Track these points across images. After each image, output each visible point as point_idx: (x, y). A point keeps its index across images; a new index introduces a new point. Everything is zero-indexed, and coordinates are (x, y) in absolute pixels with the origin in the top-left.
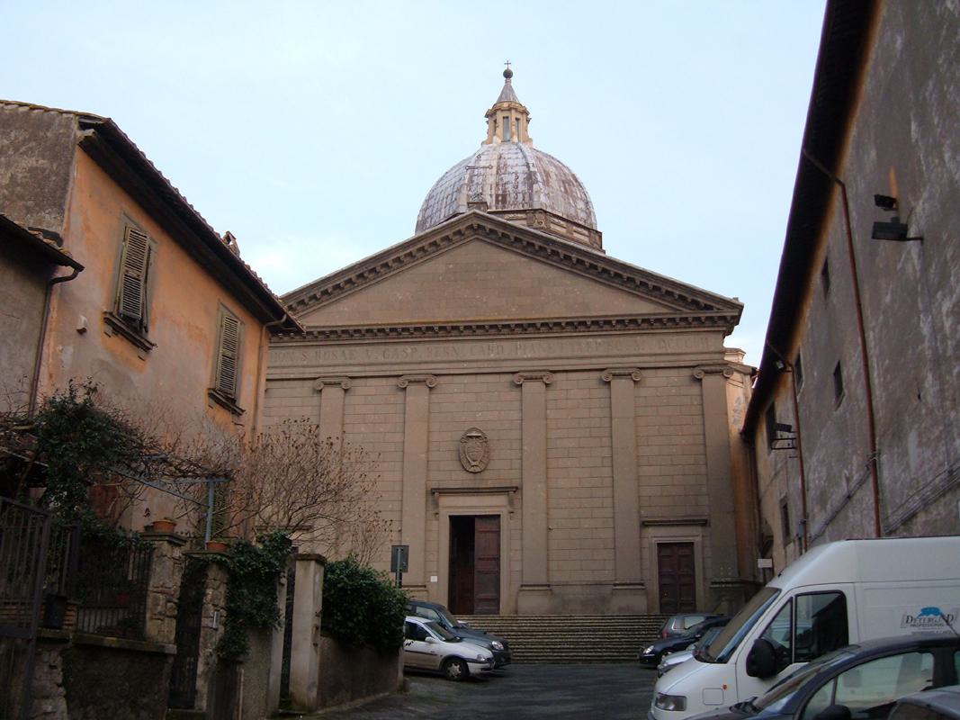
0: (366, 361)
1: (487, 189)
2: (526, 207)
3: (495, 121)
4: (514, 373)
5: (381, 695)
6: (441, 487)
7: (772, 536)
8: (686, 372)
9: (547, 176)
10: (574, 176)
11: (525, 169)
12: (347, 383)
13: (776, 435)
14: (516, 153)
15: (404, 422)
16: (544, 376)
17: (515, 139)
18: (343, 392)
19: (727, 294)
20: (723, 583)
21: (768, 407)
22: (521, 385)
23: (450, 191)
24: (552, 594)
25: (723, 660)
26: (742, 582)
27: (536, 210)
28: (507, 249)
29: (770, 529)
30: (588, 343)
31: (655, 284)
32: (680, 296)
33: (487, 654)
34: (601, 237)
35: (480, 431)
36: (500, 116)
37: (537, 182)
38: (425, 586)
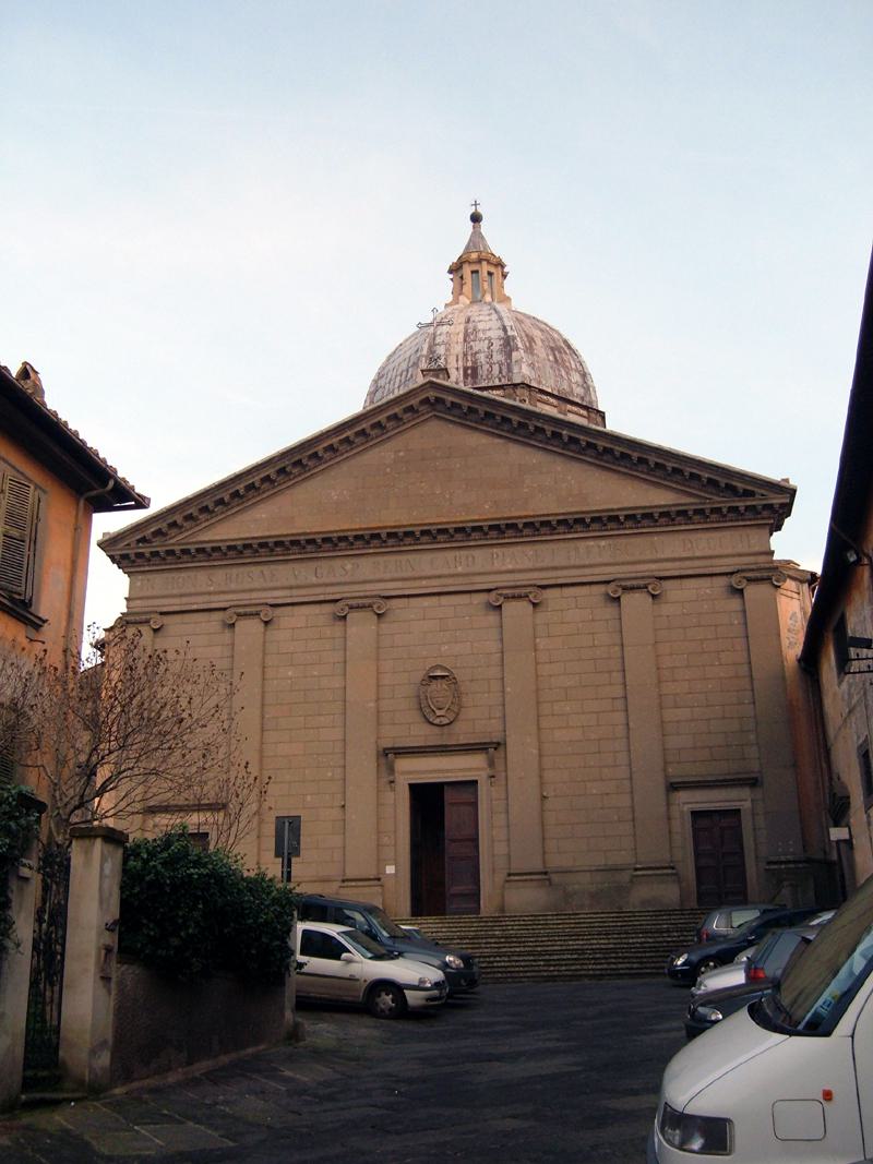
0: (293, 582)
1: (452, 360)
2: (505, 381)
3: (462, 277)
4: (489, 591)
5: (250, 1050)
6: (396, 746)
7: (848, 797)
8: (722, 581)
9: (530, 343)
10: (565, 342)
11: (501, 333)
12: (268, 613)
13: (847, 653)
14: (489, 315)
15: (345, 662)
16: (531, 594)
17: (488, 298)
18: (263, 625)
19: (773, 474)
20: (782, 863)
21: (838, 616)
22: (500, 606)
23: (404, 366)
24: (550, 884)
25: (820, 1027)
26: (808, 861)
27: (516, 385)
28: (476, 429)
29: (846, 788)
30: (588, 547)
31: (675, 465)
32: (709, 480)
33: (436, 975)
34: (603, 418)
35: (445, 669)
36: (467, 270)
37: (517, 349)
38: (379, 879)
